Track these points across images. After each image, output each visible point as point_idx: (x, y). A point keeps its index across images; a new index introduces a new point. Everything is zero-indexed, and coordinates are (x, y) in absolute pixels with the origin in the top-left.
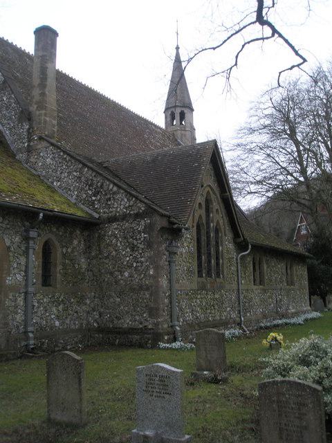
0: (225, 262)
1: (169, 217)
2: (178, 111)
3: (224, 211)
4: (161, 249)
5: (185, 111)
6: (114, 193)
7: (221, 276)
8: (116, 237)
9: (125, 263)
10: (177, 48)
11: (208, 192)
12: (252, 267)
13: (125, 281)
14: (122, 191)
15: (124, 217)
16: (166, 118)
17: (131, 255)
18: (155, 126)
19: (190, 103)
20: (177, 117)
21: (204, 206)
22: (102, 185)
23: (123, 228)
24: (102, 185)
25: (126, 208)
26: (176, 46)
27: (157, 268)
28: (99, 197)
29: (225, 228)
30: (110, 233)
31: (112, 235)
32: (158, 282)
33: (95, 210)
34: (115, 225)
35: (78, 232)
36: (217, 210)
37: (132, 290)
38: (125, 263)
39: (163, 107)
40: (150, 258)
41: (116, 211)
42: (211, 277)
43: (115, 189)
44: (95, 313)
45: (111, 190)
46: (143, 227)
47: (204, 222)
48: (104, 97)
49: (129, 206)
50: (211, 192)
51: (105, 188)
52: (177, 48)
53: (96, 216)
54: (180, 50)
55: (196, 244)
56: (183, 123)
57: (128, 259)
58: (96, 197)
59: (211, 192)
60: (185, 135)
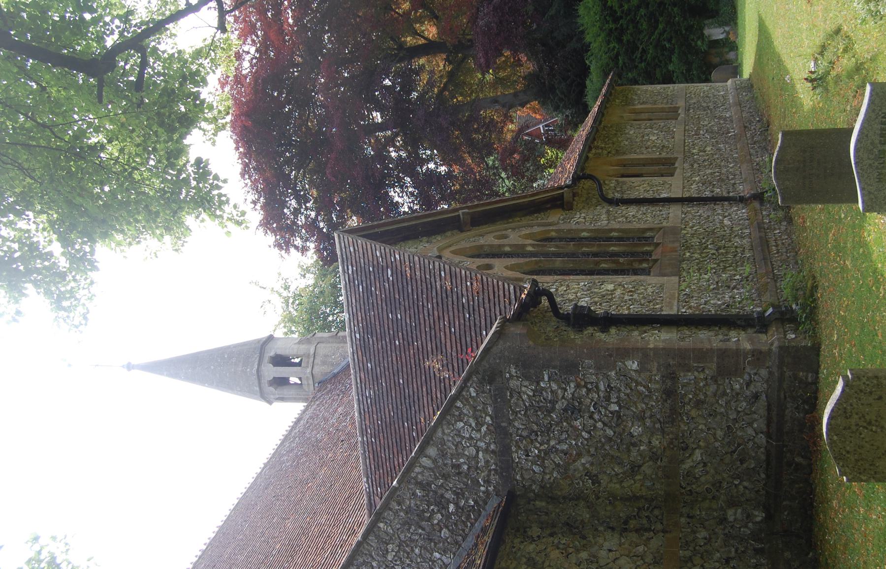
0: (617, 226)
1: (505, 322)
2: (271, 371)
3: (499, 226)
4: (579, 342)
5: (272, 354)
6: (443, 454)
7: (648, 234)
8: (547, 453)
9: (610, 432)
10: (130, 367)
11: (453, 252)
12: (633, 179)
13: (652, 434)
14: (439, 434)
15: (500, 432)
16: (282, 399)
17: (591, 417)
18: (298, 420)
19: (259, 341)
20: (282, 372)
21: (487, 261)
22: (420, 484)
23: (525, 434)
24: (420, 484)
25: (479, 424)
26: (125, 370)
27: (625, 353)
28: (449, 495)
29: (539, 225)
30: (536, 469)
31: (542, 465)
32: (655, 350)
33: (477, 509)
34: (518, 456)
35: (528, 66)
36: (499, 238)
37: (674, 416)
38: (610, 432)
39: (260, 405)
40: (599, 368)
41: (486, 451)
42: (649, 253)
43: (432, 451)
44: (731, 519)
45: (434, 461)
46: (526, 383)
47: (521, 260)
48: (221, 528)
49: (476, 418)
50: (452, 249)
51: (427, 476)
52: (130, 367)
53: (494, 503)
54: (134, 362)
55: (571, 277)
56: (297, 360)
57: (599, 425)
58: (448, 502)
59: (452, 249)
60: (326, 356)
